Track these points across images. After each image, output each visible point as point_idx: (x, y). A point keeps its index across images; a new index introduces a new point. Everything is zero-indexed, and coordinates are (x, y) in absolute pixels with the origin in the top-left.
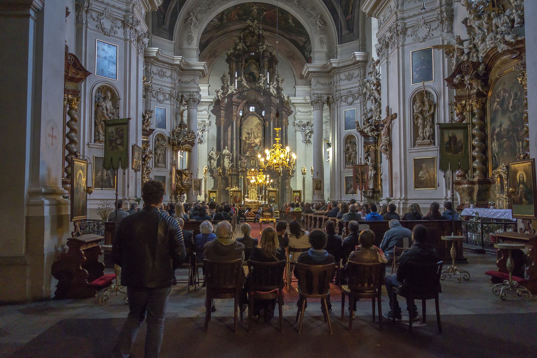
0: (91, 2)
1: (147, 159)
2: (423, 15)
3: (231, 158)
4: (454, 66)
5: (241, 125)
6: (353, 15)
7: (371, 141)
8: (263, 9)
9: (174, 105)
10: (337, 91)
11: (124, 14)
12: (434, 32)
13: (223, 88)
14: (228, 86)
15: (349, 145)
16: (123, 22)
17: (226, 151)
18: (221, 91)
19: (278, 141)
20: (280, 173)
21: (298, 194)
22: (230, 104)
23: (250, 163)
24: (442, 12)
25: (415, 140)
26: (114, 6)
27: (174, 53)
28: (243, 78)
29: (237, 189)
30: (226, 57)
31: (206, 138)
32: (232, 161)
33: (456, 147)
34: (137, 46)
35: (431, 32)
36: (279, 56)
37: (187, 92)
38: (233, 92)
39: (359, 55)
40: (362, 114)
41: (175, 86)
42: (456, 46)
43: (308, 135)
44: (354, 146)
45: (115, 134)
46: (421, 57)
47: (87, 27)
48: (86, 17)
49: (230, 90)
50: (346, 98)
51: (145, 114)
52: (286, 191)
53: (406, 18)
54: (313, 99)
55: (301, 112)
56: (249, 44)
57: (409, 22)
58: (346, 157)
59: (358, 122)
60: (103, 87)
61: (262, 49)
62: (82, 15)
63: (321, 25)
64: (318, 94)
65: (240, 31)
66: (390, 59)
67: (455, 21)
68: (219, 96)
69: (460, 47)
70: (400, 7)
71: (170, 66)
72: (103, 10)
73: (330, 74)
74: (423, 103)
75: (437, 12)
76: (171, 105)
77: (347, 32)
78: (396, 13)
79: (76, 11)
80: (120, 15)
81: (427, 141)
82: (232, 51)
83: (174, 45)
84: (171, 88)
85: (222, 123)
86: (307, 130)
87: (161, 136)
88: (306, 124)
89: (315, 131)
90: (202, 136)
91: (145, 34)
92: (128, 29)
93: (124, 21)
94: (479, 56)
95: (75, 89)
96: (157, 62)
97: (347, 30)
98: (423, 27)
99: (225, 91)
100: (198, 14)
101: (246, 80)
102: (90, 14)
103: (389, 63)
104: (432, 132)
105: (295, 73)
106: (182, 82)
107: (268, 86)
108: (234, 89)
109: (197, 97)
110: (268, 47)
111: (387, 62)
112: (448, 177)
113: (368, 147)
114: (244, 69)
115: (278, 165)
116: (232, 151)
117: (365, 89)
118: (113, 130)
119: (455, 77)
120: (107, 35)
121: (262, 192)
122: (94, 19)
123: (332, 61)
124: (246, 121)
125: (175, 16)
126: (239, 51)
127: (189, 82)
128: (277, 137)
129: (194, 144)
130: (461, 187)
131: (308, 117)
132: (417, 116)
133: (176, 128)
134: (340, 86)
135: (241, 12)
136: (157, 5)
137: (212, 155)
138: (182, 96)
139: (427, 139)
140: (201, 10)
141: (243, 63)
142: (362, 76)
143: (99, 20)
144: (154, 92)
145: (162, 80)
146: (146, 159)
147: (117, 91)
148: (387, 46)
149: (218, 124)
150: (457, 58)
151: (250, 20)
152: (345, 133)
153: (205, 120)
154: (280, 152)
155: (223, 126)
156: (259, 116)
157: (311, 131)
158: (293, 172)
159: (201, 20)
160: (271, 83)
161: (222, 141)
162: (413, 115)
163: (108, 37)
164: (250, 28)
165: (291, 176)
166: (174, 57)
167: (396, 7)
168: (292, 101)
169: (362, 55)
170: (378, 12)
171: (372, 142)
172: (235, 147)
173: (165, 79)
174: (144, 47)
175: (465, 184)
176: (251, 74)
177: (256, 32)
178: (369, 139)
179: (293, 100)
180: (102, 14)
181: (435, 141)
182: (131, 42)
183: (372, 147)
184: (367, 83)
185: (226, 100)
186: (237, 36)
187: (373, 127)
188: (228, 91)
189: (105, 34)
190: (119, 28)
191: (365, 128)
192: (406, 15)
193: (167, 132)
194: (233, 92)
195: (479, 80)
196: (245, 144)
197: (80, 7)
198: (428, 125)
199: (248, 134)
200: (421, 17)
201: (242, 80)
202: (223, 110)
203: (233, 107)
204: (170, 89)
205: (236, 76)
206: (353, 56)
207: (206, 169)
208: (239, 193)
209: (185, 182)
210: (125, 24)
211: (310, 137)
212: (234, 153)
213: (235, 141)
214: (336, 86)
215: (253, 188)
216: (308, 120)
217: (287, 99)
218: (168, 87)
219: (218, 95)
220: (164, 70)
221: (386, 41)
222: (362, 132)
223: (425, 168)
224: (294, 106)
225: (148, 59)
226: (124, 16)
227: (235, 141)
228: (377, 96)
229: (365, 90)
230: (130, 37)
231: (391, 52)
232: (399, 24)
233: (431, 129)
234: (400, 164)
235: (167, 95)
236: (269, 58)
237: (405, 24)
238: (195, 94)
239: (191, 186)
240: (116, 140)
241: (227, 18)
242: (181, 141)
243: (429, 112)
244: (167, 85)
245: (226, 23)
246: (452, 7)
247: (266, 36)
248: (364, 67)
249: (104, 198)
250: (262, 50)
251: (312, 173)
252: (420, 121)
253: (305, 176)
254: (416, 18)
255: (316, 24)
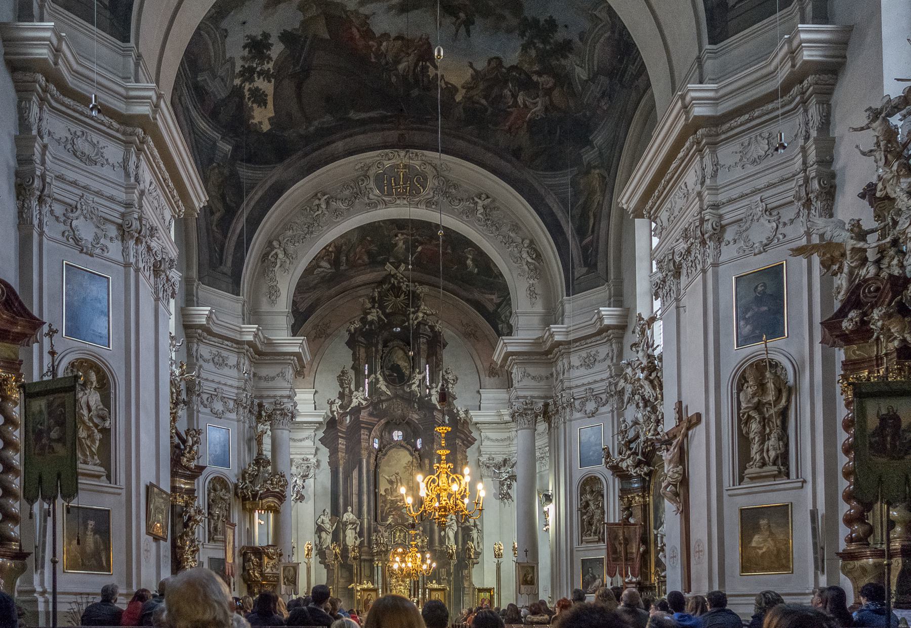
0: (48, 180)
1: (193, 525)
2: (761, 194)
3: (358, 529)
4: (842, 293)
5: (377, 466)
6: (596, 235)
7: (636, 485)
8: (417, 241)
9: (244, 422)
10: (564, 390)
11: (122, 210)
12: (788, 230)
13: (341, 396)
14: (351, 392)
15: (588, 496)
16: (120, 227)
17: (349, 516)
18: (339, 402)
19: (443, 457)
20: (451, 556)
21: (488, 594)
22: (356, 426)
23: (395, 537)
24: (807, 181)
25: (743, 468)
26: (99, 194)
27: (244, 320)
28: (379, 376)
29: (370, 586)
30: (347, 337)
31: (311, 490)
32: (360, 534)
33: (898, 443)
34: (156, 284)
35: (781, 230)
36: (447, 333)
37: (268, 397)
38: (360, 403)
39: (609, 314)
40: (616, 432)
41: (245, 383)
42: (851, 244)
43: (506, 483)
44: (600, 498)
45: (46, 416)
46: (757, 287)
47: (41, 234)
48: (40, 213)
49: (354, 400)
50: (583, 404)
51: (187, 435)
52: (463, 591)
53: (723, 204)
54: (516, 407)
55: (492, 440)
56: (391, 311)
57: (729, 214)
58: (583, 521)
59: (608, 448)
60: (82, 363)
61: (416, 319)
62: (29, 208)
63: (530, 260)
64: (525, 397)
65: (373, 285)
66: (684, 301)
67: (840, 198)
68: (334, 411)
69: (860, 245)
70: (708, 182)
71: (235, 345)
72: (77, 199)
73: (549, 356)
74: (762, 386)
75: (797, 182)
76: (238, 421)
77: (585, 270)
78: (699, 194)
79: (18, 199)
80: (114, 212)
81: (771, 469)
82: (358, 325)
83: (244, 305)
84: (238, 388)
85: (341, 462)
86: (504, 475)
87: (219, 482)
88: (502, 463)
89: (520, 476)
90: (303, 487)
91: (171, 260)
92: (132, 243)
93: (122, 226)
94: (905, 263)
95: (13, 357)
96: (209, 337)
97: (585, 266)
98: (762, 220)
99: (346, 401)
100: (289, 243)
101: (385, 379)
102: (47, 205)
103: (682, 309)
104: (783, 450)
105: (480, 366)
106: (260, 378)
107: (428, 390)
108: (363, 397)
109: (289, 406)
110: (428, 315)
111: (678, 307)
112: (822, 545)
113: (628, 498)
114: (381, 358)
115: (444, 511)
116: (360, 515)
117: (622, 381)
118: (43, 407)
119: (846, 316)
120: (86, 253)
121: (418, 592)
122: (57, 218)
123: (553, 330)
124: (386, 458)
125: (242, 246)
126: (370, 326)
127: (273, 378)
128: (443, 448)
129: (284, 497)
130: (858, 563)
131: (507, 450)
132: (749, 416)
133: (250, 466)
134: (570, 379)
135: (373, 248)
136: (197, 204)
137: (322, 523)
138: (260, 406)
139: (771, 464)
140: (295, 236)
141: (380, 347)
142: (615, 358)
143: (67, 220)
144: (205, 396)
145: (219, 371)
146: (190, 524)
147: (112, 375)
148: (677, 274)
149: (334, 466)
150: (851, 273)
151: (391, 263)
152: (580, 473)
153: (308, 456)
154: (450, 481)
155: (343, 469)
156: (411, 448)
157: (512, 476)
158: (478, 554)
159: (294, 256)
160: (434, 385)
161: (341, 496)
162: (738, 414)
163: (88, 256)
164: (392, 280)
165: (474, 564)
166: (241, 328)
167: (699, 182)
168: (475, 420)
169: (616, 313)
170: (662, 193)
171: (637, 488)
172: (365, 508)
173: (226, 371)
174: (171, 288)
175: (867, 557)
176: (396, 368)
177: (404, 287)
178: (631, 483)
179: (476, 416)
180: (74, 209)
181: (788, 469)
182: (137, 270)
183: (637, 498)
184: (628, 368)
185: (348, 418)
186: (367, 295)
187: (640, 457)
188: (351, 402)
189: (82, 250)
190: (111, 239)
191: (622, 460)
192: (722, 197)
193: (231, 473)
194: (360, 403)
195: (906, 319)
196: (385, 502)
197: (25, 189)
198: (772, 435)
199: (391, 482)
200: (757, 198)
201: (377, 380)
202: (342, 437)
203: (362, 432)
204: (236, 391)
205: (366, 373)
206: (596, 316)
207: (310, 547)
208: (373, 594)
209: (268, 570)
210: (124, 232)
211: (509, 487)
212: (363, 520)
213: (365, 498)
214: (561, 381)
215: (400, 585)
216: (505, 456)
217: (464, 415)
218: (231, 386)
219: (333, 409)
220: (225, 353)
221: (674, 262)
222: (616, 469)
223: (766, 527)
224: (478, 429)
225: (188, 327)
226: (123, 215)
227: (365, 498)
228: (648, 390)
229: (622, 383)
230: (137, 261)
231: (687, 282)
232: (706, 218)
233: (781, 443)
234: (709, 521)
235: (229, 401)
236: (429, 337)
237: (721, 217)
238: (286, 400)
239: (278, 581)
240: (49, 429)
241: (347, 260)
242: (258, 491)
243: (775, 407)
244: (230, 382)
245: (345, 270)
246: (832, 169)
247: (422, 295)
248: (620, 339)
249: (88, 591)
250: (416, 322)
251: (515, 553)
252: (754, 426)
253: (500, 559)
254: (745, 202)
255: (521, 257)
